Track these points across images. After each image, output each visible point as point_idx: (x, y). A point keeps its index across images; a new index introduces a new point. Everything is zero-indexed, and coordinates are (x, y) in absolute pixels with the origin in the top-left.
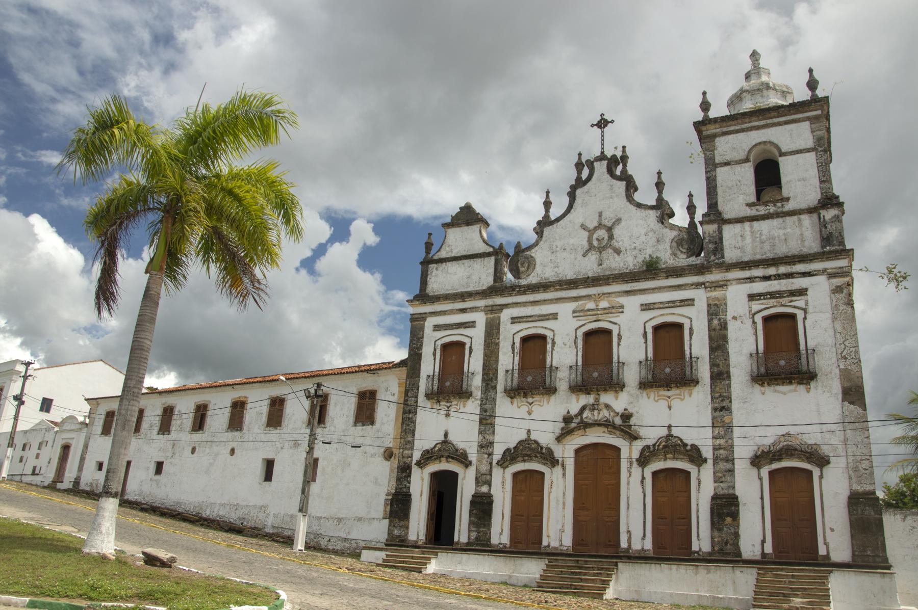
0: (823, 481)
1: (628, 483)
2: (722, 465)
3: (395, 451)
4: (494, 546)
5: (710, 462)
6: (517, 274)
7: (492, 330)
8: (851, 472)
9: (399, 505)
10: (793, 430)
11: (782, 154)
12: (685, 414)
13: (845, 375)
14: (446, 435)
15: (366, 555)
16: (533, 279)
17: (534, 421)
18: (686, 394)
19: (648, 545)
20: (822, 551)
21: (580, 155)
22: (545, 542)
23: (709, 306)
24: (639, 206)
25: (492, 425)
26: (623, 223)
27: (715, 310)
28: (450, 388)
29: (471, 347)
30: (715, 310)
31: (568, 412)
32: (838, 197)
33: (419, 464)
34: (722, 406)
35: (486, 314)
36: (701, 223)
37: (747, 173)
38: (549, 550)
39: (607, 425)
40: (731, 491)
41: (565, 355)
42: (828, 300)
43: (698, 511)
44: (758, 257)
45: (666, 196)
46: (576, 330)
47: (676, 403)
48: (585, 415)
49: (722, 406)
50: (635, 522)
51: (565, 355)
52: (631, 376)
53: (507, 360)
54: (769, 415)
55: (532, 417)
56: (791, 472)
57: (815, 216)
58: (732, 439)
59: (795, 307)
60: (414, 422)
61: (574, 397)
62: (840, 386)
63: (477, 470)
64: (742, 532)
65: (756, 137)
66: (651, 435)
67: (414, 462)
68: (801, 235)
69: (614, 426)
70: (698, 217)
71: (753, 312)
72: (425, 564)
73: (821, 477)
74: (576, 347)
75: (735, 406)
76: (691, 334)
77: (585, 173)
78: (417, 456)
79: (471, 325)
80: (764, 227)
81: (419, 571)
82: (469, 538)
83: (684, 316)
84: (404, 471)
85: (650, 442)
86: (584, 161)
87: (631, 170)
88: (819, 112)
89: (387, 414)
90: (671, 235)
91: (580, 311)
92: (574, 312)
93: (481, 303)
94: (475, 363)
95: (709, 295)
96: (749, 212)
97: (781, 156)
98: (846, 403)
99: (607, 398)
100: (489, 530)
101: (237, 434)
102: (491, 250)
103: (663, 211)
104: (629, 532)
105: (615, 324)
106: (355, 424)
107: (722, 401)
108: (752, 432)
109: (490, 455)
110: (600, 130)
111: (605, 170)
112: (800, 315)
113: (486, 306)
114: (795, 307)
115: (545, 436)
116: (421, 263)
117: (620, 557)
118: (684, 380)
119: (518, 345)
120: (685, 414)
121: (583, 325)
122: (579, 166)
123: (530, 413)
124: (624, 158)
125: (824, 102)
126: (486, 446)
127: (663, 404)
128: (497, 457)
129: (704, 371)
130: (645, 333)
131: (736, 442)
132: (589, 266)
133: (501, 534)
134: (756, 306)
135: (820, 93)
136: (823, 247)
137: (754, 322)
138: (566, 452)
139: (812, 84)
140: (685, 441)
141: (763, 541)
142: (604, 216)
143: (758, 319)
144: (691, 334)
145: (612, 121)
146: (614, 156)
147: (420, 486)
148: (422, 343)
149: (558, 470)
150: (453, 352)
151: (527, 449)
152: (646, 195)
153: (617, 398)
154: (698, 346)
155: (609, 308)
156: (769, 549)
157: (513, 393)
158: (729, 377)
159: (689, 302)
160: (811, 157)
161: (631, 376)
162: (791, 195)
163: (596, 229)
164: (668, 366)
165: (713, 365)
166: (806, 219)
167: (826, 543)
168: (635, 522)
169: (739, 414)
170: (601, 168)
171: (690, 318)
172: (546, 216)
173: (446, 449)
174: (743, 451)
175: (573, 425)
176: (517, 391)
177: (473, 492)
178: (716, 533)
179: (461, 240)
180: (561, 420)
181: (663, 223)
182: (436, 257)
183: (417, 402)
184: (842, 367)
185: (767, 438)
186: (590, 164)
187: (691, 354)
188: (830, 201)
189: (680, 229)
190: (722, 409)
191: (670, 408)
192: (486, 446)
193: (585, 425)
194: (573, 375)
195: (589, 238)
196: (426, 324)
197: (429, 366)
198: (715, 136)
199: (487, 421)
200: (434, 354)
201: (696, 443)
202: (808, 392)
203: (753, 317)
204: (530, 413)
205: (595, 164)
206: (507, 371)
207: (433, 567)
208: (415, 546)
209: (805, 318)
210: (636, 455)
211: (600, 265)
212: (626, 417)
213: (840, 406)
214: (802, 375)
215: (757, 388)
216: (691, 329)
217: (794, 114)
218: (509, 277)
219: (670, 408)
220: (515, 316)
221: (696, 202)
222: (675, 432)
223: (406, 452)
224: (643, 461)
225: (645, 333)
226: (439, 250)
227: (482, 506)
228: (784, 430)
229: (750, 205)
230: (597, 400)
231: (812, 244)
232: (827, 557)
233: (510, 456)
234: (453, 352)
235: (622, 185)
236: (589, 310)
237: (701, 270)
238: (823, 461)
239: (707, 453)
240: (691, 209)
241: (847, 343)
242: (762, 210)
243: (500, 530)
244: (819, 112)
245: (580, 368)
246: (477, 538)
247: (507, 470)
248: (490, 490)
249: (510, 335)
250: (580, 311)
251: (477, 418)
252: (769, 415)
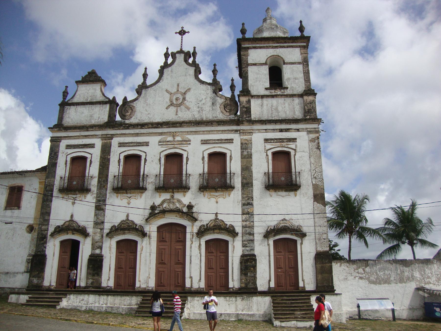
0: (303, 246)
1: (191, 247)
2: (248, 237)
3: (36, 227)
4: (104, 288)
5: (240, 235)
6: (123, 116)
7: (106, 151)
8: (317, 241)
9: (37, 262)
10: (287, 217)
11: (284, 63)
12: (226, 208)
13: (315, 187)
14: (72, 216)
15: (13, 298)
16: (133, 120)
17: (132, 208)
18: (227, 195)
19: (202, 285)
20: (301, 284)
21: (167, 49)
22: (137, 285)
23: (242, 144)
24: (202, 82)
25: (104, 210)
26: (192, 91)
27: (245, 147)
28: (76, 187)
29: (91, 160)
30: (245, 147)
31: (154, 204)
32: (314, 90)
33: (52, 235)
34: (247, 203)
35: (102, 140)
36: (239, 96)
37: (265, 70)
38: (140, 290)
39: (178, 211)
40: (252, 252)
41: (153, 169)
42: (307, 145)
43: (232, 264)
44: (270, 118)
45: (218, 78)
46: (160, 153)
47: (221, 200)
48: (164, 206)
49: (247, 203)
50: (195, 271)
51: (153, 169)
52: (194, 183)
53: (115, 169)
54: (273, 209)
55: (130, 206)
56: (285, 239)
57: (301, 99)
58: (253, 222)
59: (290, 148)
60: (50, 208)
61: (157, 195)
62: (312, 193)
63: (93, 239)
64: (258, 276)
65: (271, 52)
66: (205, 218)
67: (49, 233)
68: (290, 108)
69: (183, 212)
70: (237, 93)
71: (267, 149)
72: (58, 302)
73: (302, 244)
74: (160, 164)
75: (255, 203)
76: (231, 160)
77: (170, 60)
78: (51, 229)
79: (92, 146)
80: (274, 101)
81: (54, 307)
82: (87, 284)
83: (227, 149)
84: (41, 240)
85: (205, 223)
86: (170, 52)
87: (198, 61)
88: (305, 44)
89: (30, 202)
90: (220, 101)
91: (163, 142)
92: (160, 142)
93: (99, 133)
94: (93, 170)
95: (242, 137)
96: (267, 93)
97: (284, 64)
98: (315, 203)
99: (178, 196)
100: (101, 278)
101: (16, 212)
102: (107, 100)
103: (216, 86)
104: (191, 277)
105: (185, 151)
106: (6, 209)
107: (248, 199)
108: (264, 218)
109: (102, 229)
110: (180, 36)
111: (183, 59)
112: (292, 153)
113: (102, 135)
114: (290, 148)
115: (138, 218)
116: (59, 105)
117: (186, 293)
118: (225, 187)
119: (122, 161)
120: (226, 208)
121: (166, 150)
122: (166, 55)
123: (129, 204)
124: (194, 54)
125: (308, 39)
126: (99, 224)
127: (213, 200)
128: (106, 231)
129: (237, 182)
130: (203, 158)
131: (256, 224)
132: (170, 115)
133: (109, 280)
134: (268, 146)
135: (306, 34)
136: (305, 116)
137: (267, 155)
138: (152, 229)
139: (301, 29)
140: (226, 223)
141: (270, 281)
142: (180, 87)
143: (270, 153)
144: (231, 160)
145: (188, 32)
146: (189, 52)
147: (53, 250)
148: (58, 156)
149: (146, 239)
150: (79, 162)
151: (127, 226)
152: (206, 76)
153: (184, 196)
154: (234, 166)
155: (181, 141)
156: (272, 285)
157: (117, 190)
158: (252, 186)
159: (230, 141)
160: (300, 67)
161: (194, 183)
162: (289, 86)
163: (175, 93)
164: (216, 180)
165: (243, 178)
166: (297, 100)
167: (303, 280)
168: (195, 271)
169: (257, 209)
170: (180, 58)
171: (231, 150)
172: (144, 82)
173: (71, 227)
174: (259, 230)
175: (156, 212)
176: (121, 189)
177: (90, 254)
178: (244, 277)
179: (91, 91)
180: (149, 207)
181: (216, 94)
182: (70, 102)
183: (52, 194)
184: (314, 183)
185: (273, 221)
186: (174, 55)
187: (230, 171)
188: (310, 92)
189: (226, 98)
190: (249, 204)
191: (217, 202)
192: (99, 224)
193: (164, 212)
194: (158, 181)
195: (170, 98)
196: (61, 144)
197: (62, 170)
198: (248, 48)
199: (100, 207)
200: (66, 164)
201: (232, 224)
202: (296, 196)
203: (267, 153)
204: (129, 204)
205: (177, 55)
206: (115, 176)
207: (64, 303)
208: (49, 289)
209: (295, 155)
210: (195, 230)
211: (177, 115)
212: (190, 207)
213: (312, 204)
214: (291, 186)
215: (268, 192)
216: (231, 156)
217: (292, 43)
218: (118, 118)
219: (217, 202)
220: (122, 142)
221: (235, 83)
222: (220, 217)
223: (43, 227)
224: (201, 233)
225: (203, 158)
226: (72, 98)
227: (96, 263)
228: (282, 217)
229: (266, 89)
230: (172, 197)
231: (299, 114)
232: (304, 287)
233: (114, 231)
234: (79, 162)
235: (192, 70)
236: (168, 141)
237: (238, 122)
238: (303, 235)
239: (239, 229)
240: (232, 87)
241: (316, 170)
242: (273, 92)
243: (108, 278)
244: (305, 44)
245: (162, 176)
246: (92, 283)
247: (113, 239)
248: (101, 252)
249: (117, 154)
250: (163, 142)
251: (94, 205)
252: (273, 209)
